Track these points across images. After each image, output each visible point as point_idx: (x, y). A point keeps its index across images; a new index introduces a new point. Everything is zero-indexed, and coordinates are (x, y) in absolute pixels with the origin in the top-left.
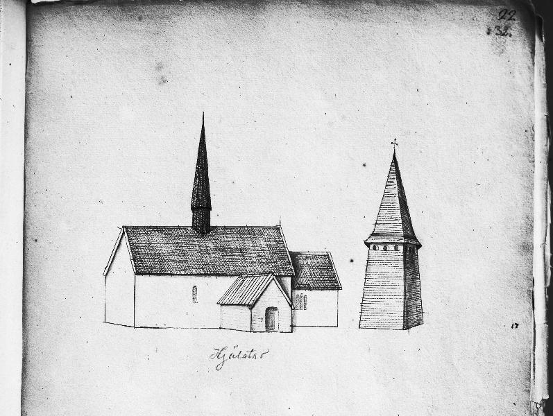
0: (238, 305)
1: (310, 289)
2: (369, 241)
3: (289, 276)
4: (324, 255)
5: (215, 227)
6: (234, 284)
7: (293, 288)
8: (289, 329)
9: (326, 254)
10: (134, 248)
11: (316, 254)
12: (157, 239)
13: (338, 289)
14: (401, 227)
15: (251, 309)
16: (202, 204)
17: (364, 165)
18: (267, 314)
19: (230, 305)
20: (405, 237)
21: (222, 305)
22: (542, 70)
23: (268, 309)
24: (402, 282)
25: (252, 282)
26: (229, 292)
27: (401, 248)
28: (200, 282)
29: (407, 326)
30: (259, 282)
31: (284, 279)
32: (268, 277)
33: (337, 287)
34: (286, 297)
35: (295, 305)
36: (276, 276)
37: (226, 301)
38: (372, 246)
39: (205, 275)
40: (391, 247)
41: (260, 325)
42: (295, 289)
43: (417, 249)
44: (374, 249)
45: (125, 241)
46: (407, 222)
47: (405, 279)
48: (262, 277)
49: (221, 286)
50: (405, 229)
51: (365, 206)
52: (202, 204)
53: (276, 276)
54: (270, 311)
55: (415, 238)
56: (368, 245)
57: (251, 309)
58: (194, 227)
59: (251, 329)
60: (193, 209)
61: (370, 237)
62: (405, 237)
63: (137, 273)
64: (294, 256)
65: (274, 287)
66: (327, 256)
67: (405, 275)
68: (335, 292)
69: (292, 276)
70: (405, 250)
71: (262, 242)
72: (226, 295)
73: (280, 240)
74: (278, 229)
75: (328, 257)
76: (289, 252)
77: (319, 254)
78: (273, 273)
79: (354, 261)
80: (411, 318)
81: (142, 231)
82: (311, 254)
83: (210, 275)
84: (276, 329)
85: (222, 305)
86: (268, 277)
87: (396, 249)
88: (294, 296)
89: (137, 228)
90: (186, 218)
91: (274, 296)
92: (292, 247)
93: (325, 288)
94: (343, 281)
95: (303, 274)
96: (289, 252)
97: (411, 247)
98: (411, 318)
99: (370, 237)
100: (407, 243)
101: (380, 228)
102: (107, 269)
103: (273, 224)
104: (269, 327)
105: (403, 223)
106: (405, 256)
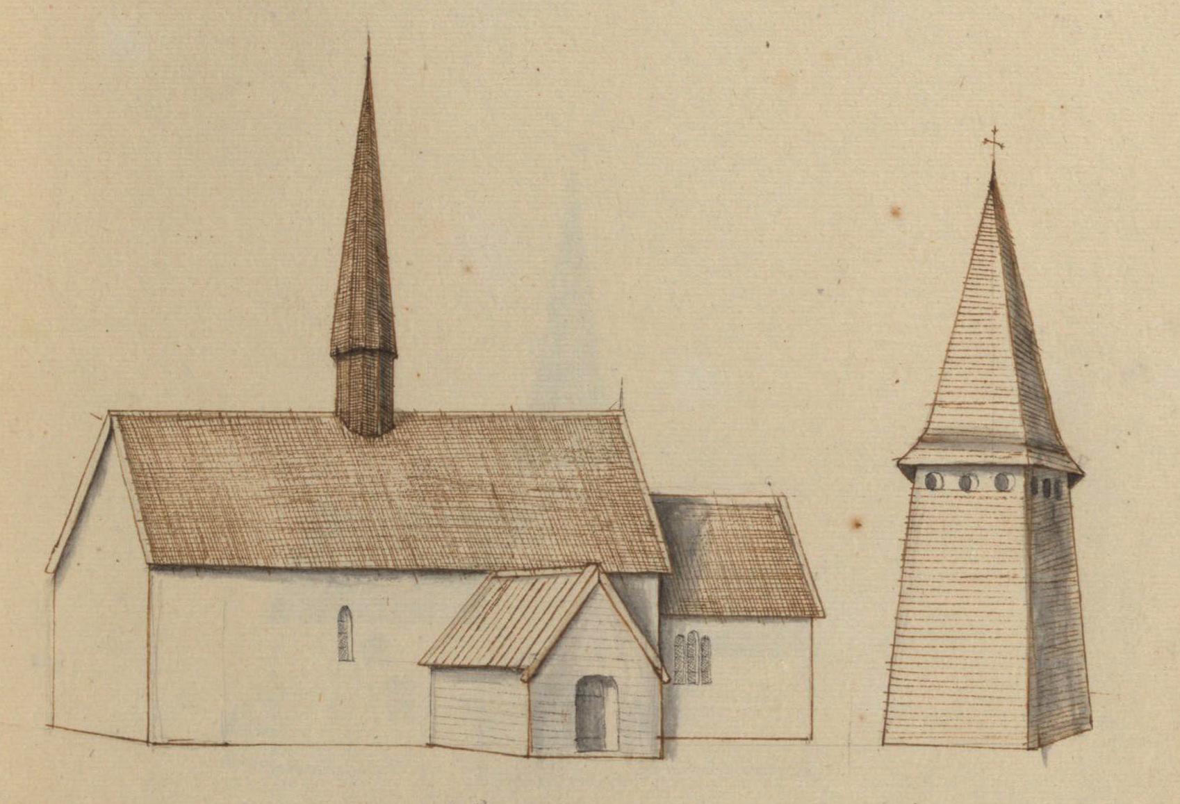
0: (487, 667)
1: (719, 617)
2: (914, 459)
3: (649, 574)
4: (767, 506)
5: (409, 416)
6: (473, 603)
7: (664, 615)
8: (648, 745)
9: (770, 501)
10: (144, 484)
11: (740, 501)
12: (226, 458)
13: (812, 618)
14: (1018, 414)
15: (529, 681)
16: (367, 348)
17: (896, 213)
18: (580, 696)
19: (460, 667)
20: (1033, 445)
21: (435, 668)
22: (476, 685)
23: (584, 681)
24: (1020, 593)
25: (532, 593)
26: (455, 625)
27: (1017, 483)
28: (362, 595)
29: (1039, 741)
30: (553, 593)
31: (637, 583)
32: (583, 580)
33: (808, 611)
34: (643, 640)
35: (671, 668)
36: (610, 575)
37: (449, 656)
38: (921, 476)
39: (378, 571)
40: (986, 481)
41: (561, 733)
42: (672, 616)
43: (1071, 485)
44: (931, 485)
45: (116, 463)
46: (1035, 398)
47: (1031, 583)
48: (562, 580)
49: (417, 614)
50: (1030, 418)
51: (903, 351)
52: (367, 348)
53: (610, 575)
54: (589, 690)
55: (1061, 451)
56: (910, 471)
57: (529, 681)
58: (338, 414)
59: (530, 748)
60: (337, 356)
61: (914, 448)
62: (1033, 445)
63: (157, 567)
64: (667, 507)
65: (604, 608)
66: (776, 509)
67: (1031, 570)
68: (804, 626)
69: (662, 577)
70: (1031, 488)
71: (563, 464)
72: (448, 635)
73: (622, 447)
74: (613, 420)
75: (780, 512)
76: (652, 495)
77: (747, 501)
78: (598, 565)
79: (861, 529)
80: (1055, 703)
81: (171, 431)
82: (724, 501)
83: (395, 572)
84: (610, 740)
85: (435, 668)
86: (583, 580)
87: (1001, 486)
88: (671, 639)
89: (151, 417)
90: (316, 386)
91: (608, 644)
92: (663, 477)
93: (770, 615)
94: (828, 591)
95: (682, 569)
96: (652, 495)
97: (1050, 481)
98: (1055, 703)
99: (914, 448)
100: (1036, 466)
101: (948, 420)
102: (59, 550)
103: (604, 403)
104: (588, 739)
105: (1021, 403)
106: (1029, 509)
